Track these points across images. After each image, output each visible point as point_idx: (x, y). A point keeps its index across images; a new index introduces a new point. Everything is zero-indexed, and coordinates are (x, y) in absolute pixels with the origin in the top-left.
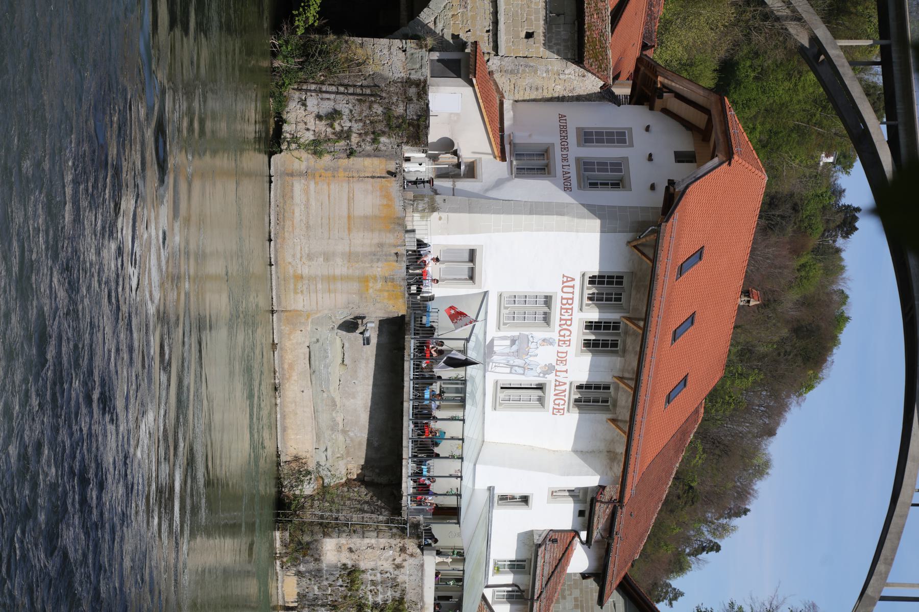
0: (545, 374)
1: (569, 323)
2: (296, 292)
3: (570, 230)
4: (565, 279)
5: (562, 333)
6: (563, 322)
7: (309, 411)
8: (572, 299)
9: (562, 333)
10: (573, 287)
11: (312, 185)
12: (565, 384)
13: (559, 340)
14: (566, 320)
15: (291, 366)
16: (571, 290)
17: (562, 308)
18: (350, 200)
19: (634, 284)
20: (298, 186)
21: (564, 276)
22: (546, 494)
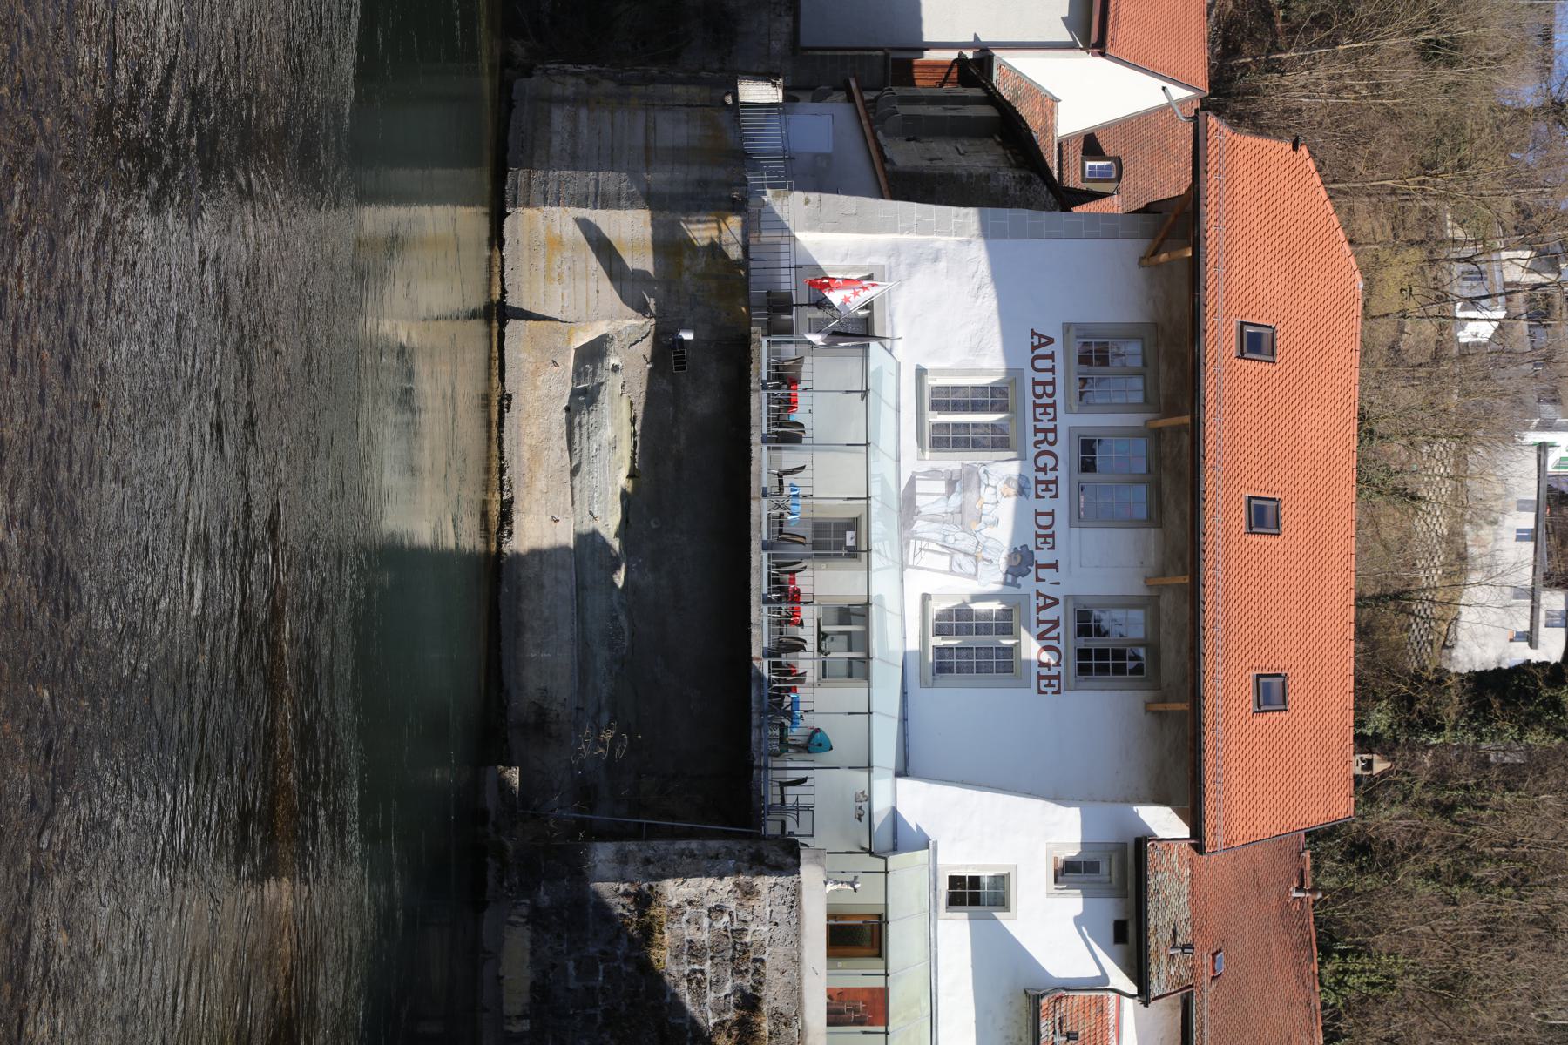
1: (1051, 437)
2: (548, 278)
5: (1042, 461)
6: (1041, 436)
8: (1053, 383)
9: (1042, 461)
10: (1052, 357)
12: (1056, 602)
13: (1038, 482)
14: (1046, 431)
15: (536, 452)
16: (1047, 364)
17: (1036, 406)
19: (1162, 350)
20: (559, 118)
21: (1033, 334)
22: (1045, 873)
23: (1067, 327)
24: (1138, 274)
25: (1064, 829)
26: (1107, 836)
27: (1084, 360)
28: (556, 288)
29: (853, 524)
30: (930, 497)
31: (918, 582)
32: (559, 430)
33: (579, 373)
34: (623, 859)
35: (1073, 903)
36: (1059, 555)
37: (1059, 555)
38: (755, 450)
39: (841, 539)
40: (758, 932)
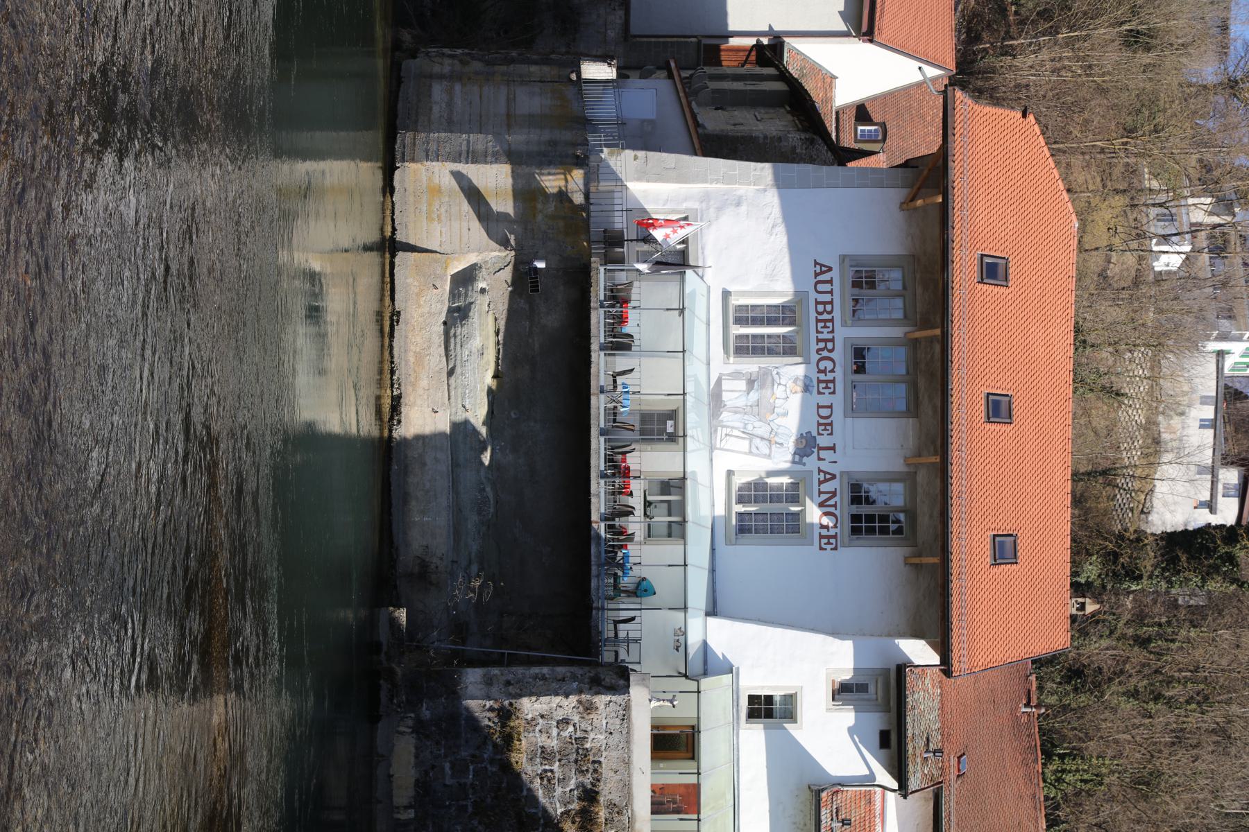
0: (801, 457)
1: (830, 345)
2: (429, 218)
3: (818, 185)
4: (818, 269)
5: (822, 365)
6: (822, 345)
7: (444, 467)
8: (831, 303)
9: (822, 365)
10: (830, 282)
11: (458, 87)
12: (834, 477)
14: (826, 341)
15: (419, 357)
16: (827, 287)
17: (818, 321)
18: (510, 101)
19: (918, 276)
20: (438, 91)
21: (816, 263)
22: (825, 692)
23: (843, 258)
24: (899, 216)
25: (839, 658)
26: (875, 663)
27: (856, 284)
28: (436, 227)
29: (672, 415)
30: (734, 393)
31: (723, 462)
32: (438, 340)
33: (454, 295)
34: (489, 682)
35: (847, 716)
36: (837, 439)
37: (837, 439)
38: (594, 356)
39: (662, 427)
40: (597, 739)
